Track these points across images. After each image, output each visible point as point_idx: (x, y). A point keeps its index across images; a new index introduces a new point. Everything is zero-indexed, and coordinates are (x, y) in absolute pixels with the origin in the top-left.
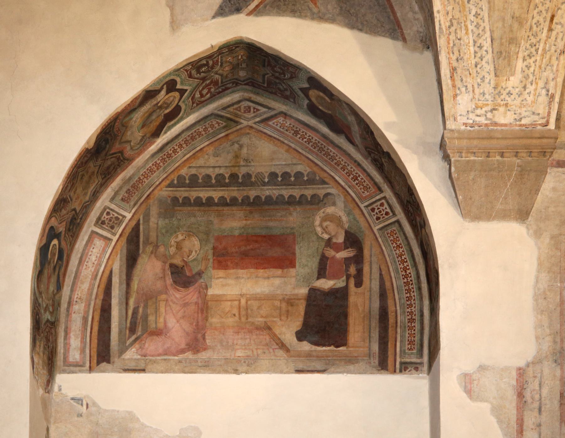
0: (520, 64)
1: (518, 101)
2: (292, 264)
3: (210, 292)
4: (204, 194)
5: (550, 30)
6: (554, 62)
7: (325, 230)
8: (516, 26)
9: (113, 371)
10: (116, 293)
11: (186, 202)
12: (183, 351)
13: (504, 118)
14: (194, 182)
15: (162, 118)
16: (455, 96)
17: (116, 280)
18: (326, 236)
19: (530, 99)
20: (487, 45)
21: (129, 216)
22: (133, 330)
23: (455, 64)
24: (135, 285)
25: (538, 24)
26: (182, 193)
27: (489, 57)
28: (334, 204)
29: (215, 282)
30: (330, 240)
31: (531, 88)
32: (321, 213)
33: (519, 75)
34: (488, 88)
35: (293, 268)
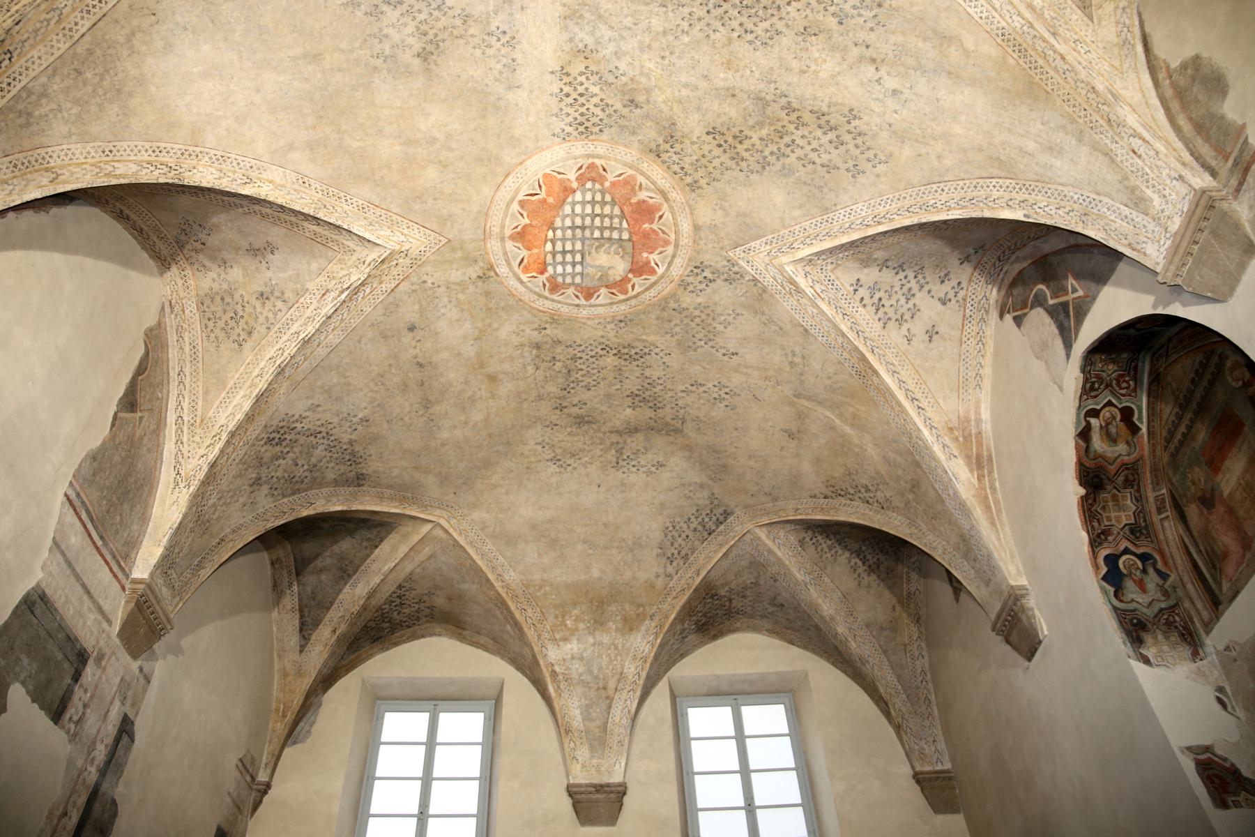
0: (1149, 192)
1: (1170, 206)
2: (1243, 425)
3: (1225, 494)
4: (1179, 436)
5: (1140, 157)
6: (1160, 163)
7: (1237, 380)
8: (1126, 183)
9: (1226, 608)
10: (1192, 550)
11: (1177, 449)
12: (1244, 556)
13: (1176, 224)
14: (1171, 433)
15: (1122, 425)
16: (1145, 254)
17: (1186, 540)
18: (1240, 383)
19: (1174, 197)
20: (1126, 211)
21: (1164, 491)
22: (1214, 567)
23: (1126, 242)
24: (1195, 534)
25: (1132, 165)
26: (1172, 446)
27: (1135, 213)
28: (1227, 357)
29: (1222, 485)
30: (1244, 383)
31: (1167, 192)
32: (1227, 372)
33: (1155, 197)
34: (1151, 226)
35: (592, 748)
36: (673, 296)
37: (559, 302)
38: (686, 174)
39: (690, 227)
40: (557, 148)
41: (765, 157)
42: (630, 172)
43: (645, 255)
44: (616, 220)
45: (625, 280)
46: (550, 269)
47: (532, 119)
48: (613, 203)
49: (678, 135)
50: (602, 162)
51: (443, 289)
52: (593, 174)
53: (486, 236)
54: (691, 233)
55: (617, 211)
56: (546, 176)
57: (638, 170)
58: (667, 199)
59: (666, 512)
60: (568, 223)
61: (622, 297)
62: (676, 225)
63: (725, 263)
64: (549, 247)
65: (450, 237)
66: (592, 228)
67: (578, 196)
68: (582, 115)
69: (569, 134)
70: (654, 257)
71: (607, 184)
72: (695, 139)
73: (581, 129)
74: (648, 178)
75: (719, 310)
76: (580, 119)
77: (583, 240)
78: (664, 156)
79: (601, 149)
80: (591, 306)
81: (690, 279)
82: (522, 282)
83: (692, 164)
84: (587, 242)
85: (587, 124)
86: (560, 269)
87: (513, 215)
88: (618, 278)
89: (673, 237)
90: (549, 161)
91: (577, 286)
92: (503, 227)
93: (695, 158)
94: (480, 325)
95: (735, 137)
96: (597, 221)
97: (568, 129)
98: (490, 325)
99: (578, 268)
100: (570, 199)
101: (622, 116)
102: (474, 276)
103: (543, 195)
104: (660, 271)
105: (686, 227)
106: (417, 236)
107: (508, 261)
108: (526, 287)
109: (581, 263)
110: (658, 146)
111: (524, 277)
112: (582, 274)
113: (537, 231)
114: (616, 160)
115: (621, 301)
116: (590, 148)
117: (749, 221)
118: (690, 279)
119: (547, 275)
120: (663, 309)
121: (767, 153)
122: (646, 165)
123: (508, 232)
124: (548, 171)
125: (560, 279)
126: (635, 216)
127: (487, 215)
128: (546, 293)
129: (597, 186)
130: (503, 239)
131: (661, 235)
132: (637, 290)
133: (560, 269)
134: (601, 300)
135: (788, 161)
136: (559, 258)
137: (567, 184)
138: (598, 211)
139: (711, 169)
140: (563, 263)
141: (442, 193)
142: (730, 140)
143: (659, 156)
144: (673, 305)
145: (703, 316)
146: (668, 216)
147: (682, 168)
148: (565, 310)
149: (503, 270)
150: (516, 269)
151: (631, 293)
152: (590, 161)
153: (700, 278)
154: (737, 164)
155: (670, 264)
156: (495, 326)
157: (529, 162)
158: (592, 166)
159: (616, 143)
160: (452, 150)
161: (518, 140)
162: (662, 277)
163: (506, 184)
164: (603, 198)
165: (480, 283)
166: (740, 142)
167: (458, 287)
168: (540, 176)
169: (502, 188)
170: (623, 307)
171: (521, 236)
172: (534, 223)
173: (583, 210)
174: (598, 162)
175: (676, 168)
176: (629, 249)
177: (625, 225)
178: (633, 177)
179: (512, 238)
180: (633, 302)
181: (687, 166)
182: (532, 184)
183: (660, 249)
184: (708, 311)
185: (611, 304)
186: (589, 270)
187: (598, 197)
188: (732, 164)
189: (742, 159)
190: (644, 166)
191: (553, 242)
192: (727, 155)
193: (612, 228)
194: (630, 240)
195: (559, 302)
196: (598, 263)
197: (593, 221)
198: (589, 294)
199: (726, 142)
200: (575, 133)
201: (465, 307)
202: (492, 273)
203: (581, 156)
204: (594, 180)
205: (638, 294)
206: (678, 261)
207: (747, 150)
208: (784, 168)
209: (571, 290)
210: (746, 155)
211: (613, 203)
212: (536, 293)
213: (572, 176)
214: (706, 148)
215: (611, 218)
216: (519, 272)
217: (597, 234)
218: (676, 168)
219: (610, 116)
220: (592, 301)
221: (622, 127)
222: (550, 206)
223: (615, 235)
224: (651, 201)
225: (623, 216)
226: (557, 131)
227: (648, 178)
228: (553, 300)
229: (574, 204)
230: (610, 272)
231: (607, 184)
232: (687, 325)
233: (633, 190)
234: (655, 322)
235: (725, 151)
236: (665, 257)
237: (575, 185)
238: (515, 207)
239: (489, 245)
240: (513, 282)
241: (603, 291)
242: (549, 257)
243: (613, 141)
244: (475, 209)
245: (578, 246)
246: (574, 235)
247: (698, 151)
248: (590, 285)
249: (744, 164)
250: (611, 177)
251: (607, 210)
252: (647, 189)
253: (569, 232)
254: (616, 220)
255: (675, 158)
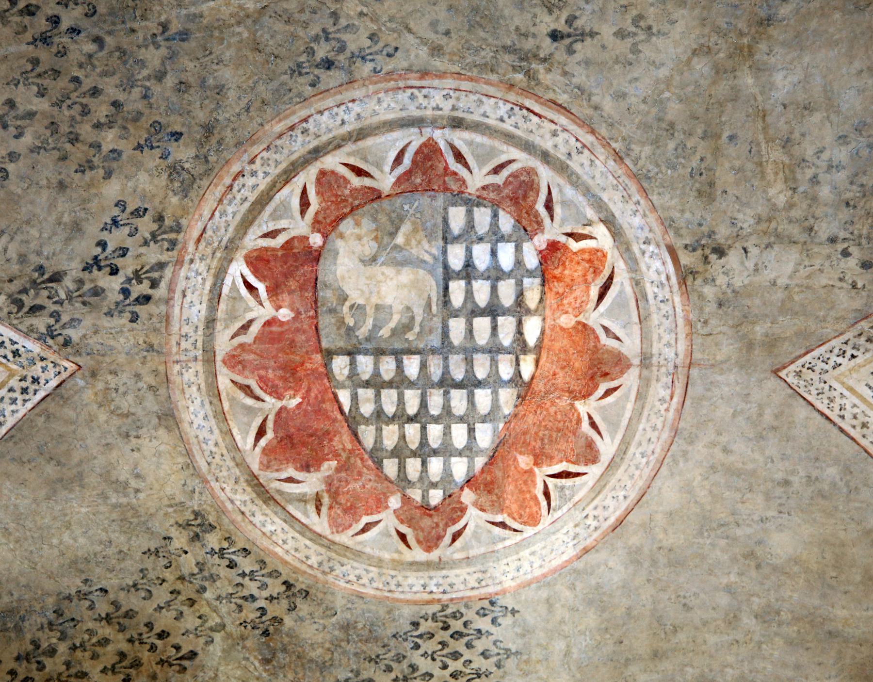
36: (185, 181)
37: (509, 138)
38: (221, 552)
39: (186, 417)
40: (509, 584)
41: (63, 637)
42: (344, 538)
43: (285, 314)
44: (367, 409)
45: (327, 225)
46: (532, 261)
47: (560, 645)
48: (377, 456)
49: (254, 639)
50: (409, 556)
51: (824, 230)
52: (427, 522)
53: (687, 371)
54: (177, 396)
55: (368, 435)
56: (533, 520)
57: (330, 545)
58: (255, 483)
59: (155, 434)
60: (483, 398)
61: (332, 162)
62: (221, 416)
63: (74, 334)
64: (532, 329)
65: (772, 383)
66: (424, 383)
67: (460, 468)
68: (456, 656)
69: (482, 613)
70: (262, 311)
71: (395, 502)
72: (218, 637)
73: (457, 625)
74: (305, 530)
75: (48, 168)
76: (459, 645)
77: (446, 347)
78: (276, 587)
79: (414, 586)
80: (417, 123)
81: (153, 255)
82: (609, 222)
83: (213, 578)
84: (435, 340)
85: (445, 636)
86: (506, 256)
87: (614, 426)
88: (347, 226)
89: (224, 382)
90: (525, 553)
91: (460, 197)
92: (641, 396)
93: (208, 595)
94: (748, 81)
95: (137, 664)
96: (412, 401)
97: (483, 624)
98: (718, 71)
99: (456, 257)
100: (480, 462)
101: (375, 660)
102: (733, 258)
103: (541, 474)
104: (238, 268)
105: (195, 412)
106: (850, 400)
107: (641, 297)
108: (599, 205)
109: (448, 275)
110: (292, 608)
111: (602, 238)
112: (448, 238)
113: (561, 379)
114: (380, 563)
115: (337, 144)
116: (435, 582)
117: (50, 470)
118: (153, 255)
119: (541, 241)
120: (208, 129)
121: (63, 648)
122: (314, 561)
123: (630, 380)
124: (529, 531)
125: (506, 223)
126: (322, 425)
127: (676, 432)
128: (545, 175)
129: (416, 495)
130: (646, 360)
131: (253, 383)
132: (290, 194)
133: (506, 256)
134: (395, 141)
135: (15, 648)
136: (507, 292)
137: (484, 499)
138: (412, 431)
139: (168, 575)
140: (496, 275)
141: (768, 497)
142: (145, 655)
143: (288, 585)
144: (183, 153)
145: (85, 130)
146: (246, 441)
147: (232, 565)
148: (494, 110)
149: (657, 267)
150: (621, 266)
151: (308, 177)
152: (434, 555)
153: (128, 266)
154: (116, 604)
155: (216, 296)
156: (701, 65)
157: (571, 553)
158: (430, 543)
159: (380, 601)
160: (729, 589)
161: (590, 603)
162: (230, 249)
163: (624, 505)
164: (402, 468)
165: (723, 233)
166: (122, 655)
167: (784, 227)
168: (546, 520)
169: (633, 495)
170: (327, 123)
171: (599, 368)
172: (564, 402)
173: (447, 433)
174: (419, 554)
175: (246, 564)
176: (326, 322)
177: (344, 397)
178: (338, 526)
179: (621, 363)
180: (299, 146)
181: (224, 572)
182: (564, 499)
183: (248, 338)
184: (78, 153)
185: (361, 134)
186: (427, 250)
187: (413, 466)
188: (133, 601)
189: (108, 618)
190: (315, 555)
191: (520, 346)
192: (142, 619)
193: (376, 383)
194: (329, 354)
195: (509, 138)
196: (406, 275)
197: (424, 405)
198: (427, 170)
199: (153, 648)
200: (470, 615)
201: (777, 154)
202: (686, 259)
203: (453, 564)
204: (426, 509)
205: (288, 176)
206: (198, 311)
207: (104, 642)
208: (18, 629)
209: (477, 179)
210: (106, 631)
211: (377, 456)
212: (574, 179)
213: (474, 518)
214: (190, 622)
215: (379, 414)
216: (615, 260)
217: (412, 366)
218: (246, 564)
219: (400, 658)
220: (415, 139)
221: (371, 637)
222: (526, 447)
223: (365, 364)
224: (291, 472)
225: (353, 421)
226: (506, 621)
227: (305, 530)
228: (528, 147)
229: (469, 450)
230: (369, 247)
231: (395, 502)
232: (128, 84)
233: (334, 495)
234: (227, 74)
235: (149, 625)
236: (232, 316)
237: (468, 497)
238: (607, 447)
239: (682, 346)
240: (633, 221)
241: (386, 181)
242: (532, 298)
243: (391, 606)
244: (699, 450)
245: (457, 328)
246: (469, 362)
247: (205, 610)
248: (423, 200)
249: (103, 608)
250: (388, 520)
251: (390, 435)
252: (302, 499)
253: (481, 373)
254: (367, 409)
255: (252, 587)
